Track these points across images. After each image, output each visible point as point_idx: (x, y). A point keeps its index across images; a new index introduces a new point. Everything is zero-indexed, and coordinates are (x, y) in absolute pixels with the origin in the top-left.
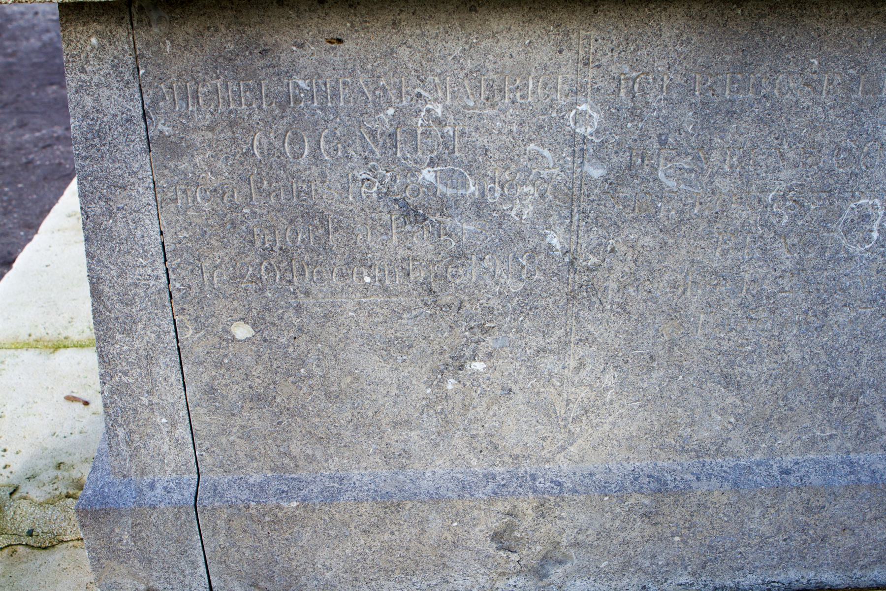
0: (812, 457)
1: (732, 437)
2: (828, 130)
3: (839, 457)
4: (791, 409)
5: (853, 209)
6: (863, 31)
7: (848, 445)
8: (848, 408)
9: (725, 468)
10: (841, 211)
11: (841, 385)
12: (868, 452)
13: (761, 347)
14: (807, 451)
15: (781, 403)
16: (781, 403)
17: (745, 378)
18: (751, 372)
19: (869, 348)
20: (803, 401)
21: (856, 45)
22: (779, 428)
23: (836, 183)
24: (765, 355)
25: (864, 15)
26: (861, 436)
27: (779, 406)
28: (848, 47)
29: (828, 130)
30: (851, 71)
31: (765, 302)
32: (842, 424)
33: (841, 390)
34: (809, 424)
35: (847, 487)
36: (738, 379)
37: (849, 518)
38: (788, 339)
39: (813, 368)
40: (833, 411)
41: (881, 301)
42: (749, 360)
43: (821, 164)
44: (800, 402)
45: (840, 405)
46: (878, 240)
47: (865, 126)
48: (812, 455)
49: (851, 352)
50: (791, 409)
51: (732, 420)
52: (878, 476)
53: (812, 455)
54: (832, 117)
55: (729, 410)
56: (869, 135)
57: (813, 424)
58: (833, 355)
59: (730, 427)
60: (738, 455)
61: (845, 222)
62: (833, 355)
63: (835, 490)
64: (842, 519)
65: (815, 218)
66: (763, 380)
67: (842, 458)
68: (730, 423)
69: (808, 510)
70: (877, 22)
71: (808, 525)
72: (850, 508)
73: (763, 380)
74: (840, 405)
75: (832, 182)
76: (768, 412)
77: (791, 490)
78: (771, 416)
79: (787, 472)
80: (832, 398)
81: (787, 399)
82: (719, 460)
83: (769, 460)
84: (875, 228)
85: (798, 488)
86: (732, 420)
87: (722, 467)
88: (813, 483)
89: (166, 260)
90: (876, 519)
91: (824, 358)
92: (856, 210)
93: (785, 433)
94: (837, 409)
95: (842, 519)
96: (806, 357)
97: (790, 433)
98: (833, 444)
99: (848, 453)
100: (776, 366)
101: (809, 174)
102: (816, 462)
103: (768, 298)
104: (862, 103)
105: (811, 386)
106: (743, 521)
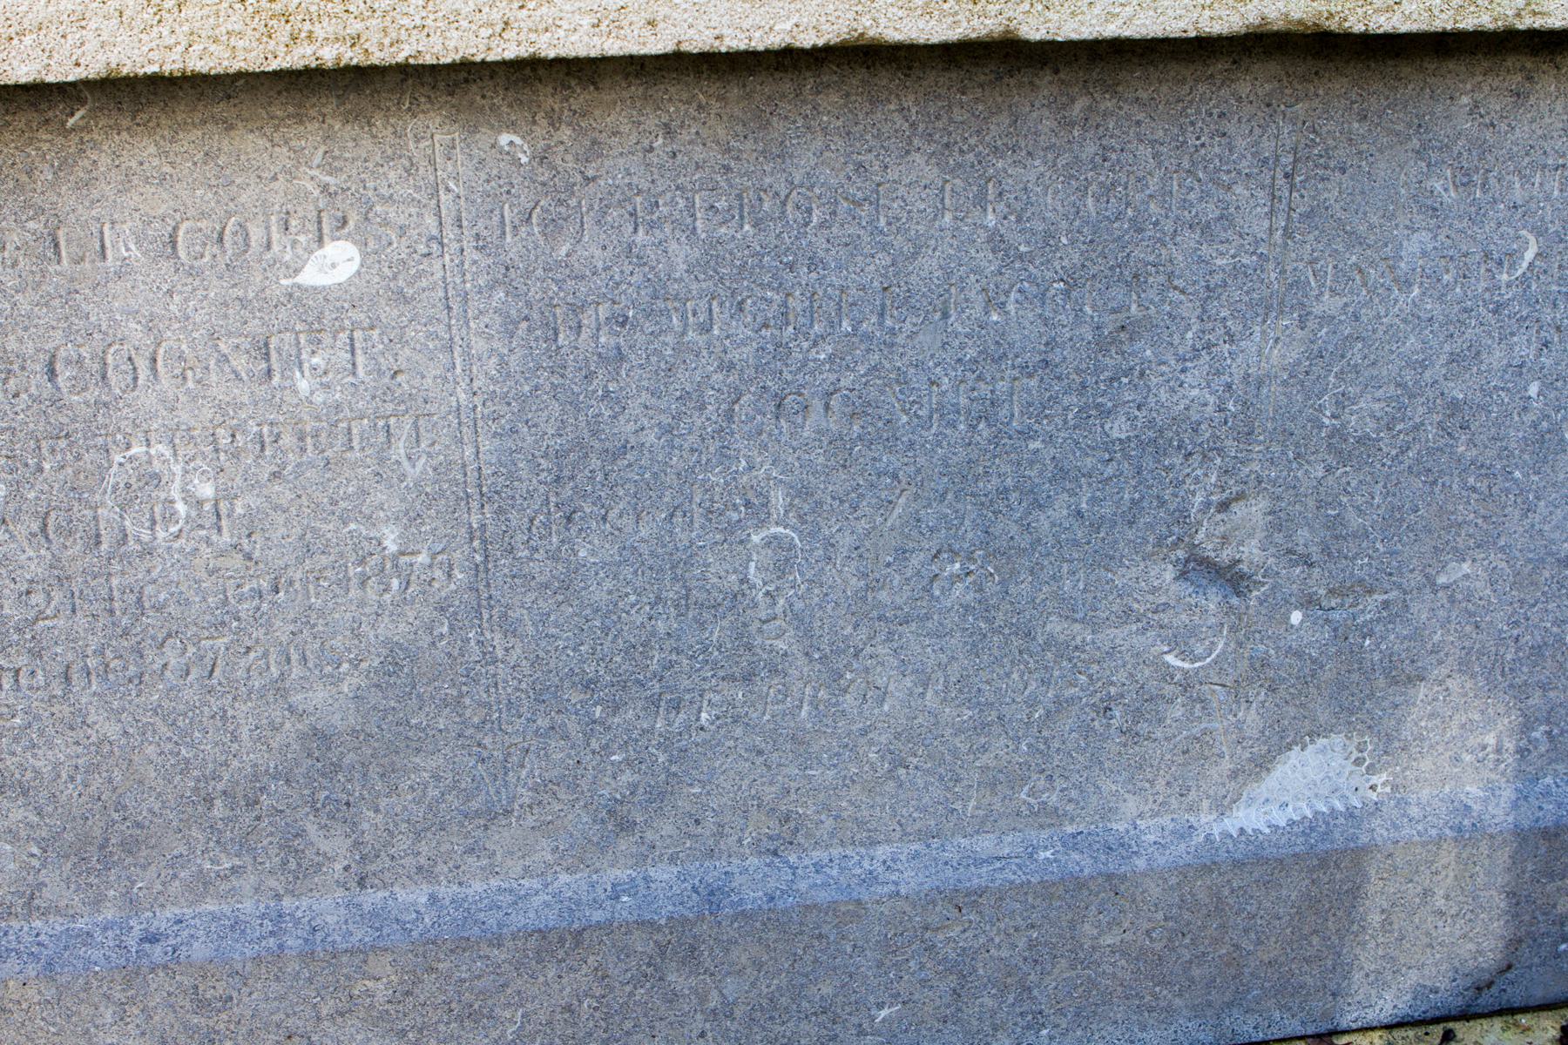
0: (211, 908)
1: (47, 880)
2: (26, 329)
3: (262, 906)
4: (138, 825)
5: (121, 464)
6: (29, 155)
7: (272, 883)
8: (247, 819)
9: (42, 938)
10: (102, 470)
11: (216, 777)
12: (314, 893)
13: (37, 718)
14: (200, 899)
15: (116, 816)
16: (116, 816)
17: (29, 775)
18: (38, 764)
19: (243, 708)
20: (156, 809)
21: (24, 178)
22: (129, 860)
23: (73, 421)
24: (50, 731)
25: (22, 125)
26: (293, 865)
27: (114, 822)
28: (11, 184)
29: (26, 329)
30: (31, 225)
31: (16, 637)
32: (244, 844)
33: (220, 786)
34: (183, 849)
35: (257, 959)
36: (18, 776)
37: (288, 1016)
38: (84, 701)
39: (151, 750)
40: (220, 825)
41: (235, 624)
42: (24, 742)
43: (33, 390)
44: (150, 810)
45: (228, 813)
46: (188, 516)
47: (93, 319)
48: (210, 906)
49: (213, 717)
50: (138, 825)
51: (35, 850)
52: (319, 936)
53: (210, 906)
54: (25, 307)
55: (23, 834)
56: (105, 334)
57: (192, 850)
58: (180, 724)
59: (35, 863)
60: (71, 912)
61: (115, 489)
62: (180, 724)
63: (239, 967)
64: (276, 1018)
65: (56, 486)
66: (64, 776)
67: (267, 907)
68: (33, 855)
69: (202, 1005)
70: (49, 137)
71: (218, 1033)
72: (282, 998)
73: (64, 776)
74: (228, 813)
75: (65, 420)
76: (97, 832)
77: (153, 970)
78: (107, 840)
79: (153, 939)
80: (209, 801)
81: (125, 807)
82: (38, 924)
83: (130, 917)
84: (176, 494)
85: (165, 967)
86: (35, 850)
87: (38, 935)
88: (194, 956)
89: (1389, 1027)
90: (342, 1015)
91: (164, 730)
92: (128, 466)
93: (144, 867)
94: (226, 820)
95: (276, 1018)
96: (131, 731)
97: (153, 868)
98: (247, 882)
99: (278, 897)
100: (80, 750)
101: (18, 409)
102: (215, 917)
103: (19, 630)
104: (72, 280)
105: (160, 781)
106: (87, 1032)
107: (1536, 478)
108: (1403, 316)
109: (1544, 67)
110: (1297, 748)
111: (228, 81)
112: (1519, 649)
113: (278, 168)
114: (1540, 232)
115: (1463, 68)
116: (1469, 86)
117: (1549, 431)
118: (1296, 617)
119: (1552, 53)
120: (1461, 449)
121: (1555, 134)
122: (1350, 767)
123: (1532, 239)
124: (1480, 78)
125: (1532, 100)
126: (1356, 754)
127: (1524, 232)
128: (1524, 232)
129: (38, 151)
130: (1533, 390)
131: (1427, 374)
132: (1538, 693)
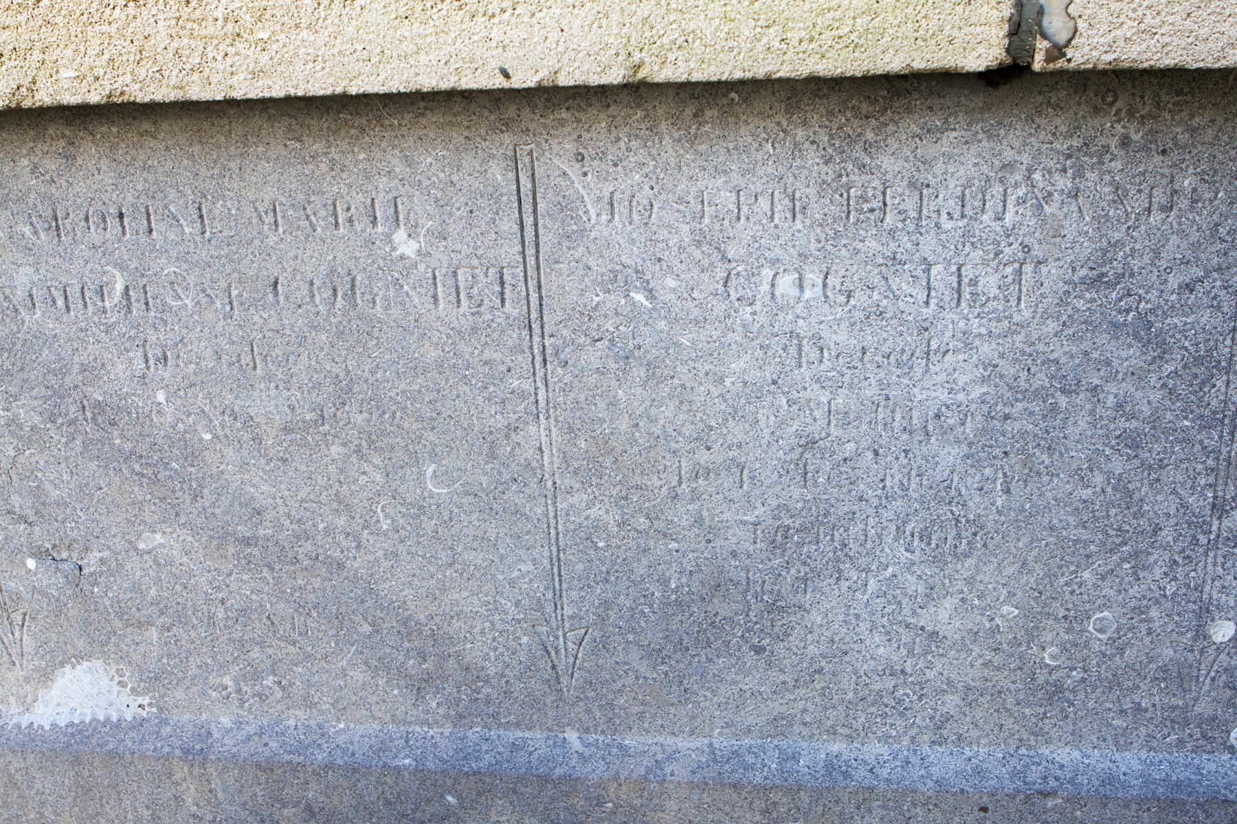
107: (193, 469)
108: (32, 333)
109: (81, 134)
110: (69, 667)
111: (1137, 75)
112: (226, 610)
113: (426, 167)
114: (123, 268)
115: (15, 137)
116: (24, 152)
117: (185, 432)
118: (31, 563)
119: (83, 122)
120: (118, 441)
121: (109, 189)
122: (116, 688)
123: (118, 275)
124: (32, 144)
125: (80, 161)
126: (117, 679)
127: (108, 268)
128: (108, 268)
129: (28, 168)
130: (161, 397)
131: (68, 380)
132: (257, 649)
